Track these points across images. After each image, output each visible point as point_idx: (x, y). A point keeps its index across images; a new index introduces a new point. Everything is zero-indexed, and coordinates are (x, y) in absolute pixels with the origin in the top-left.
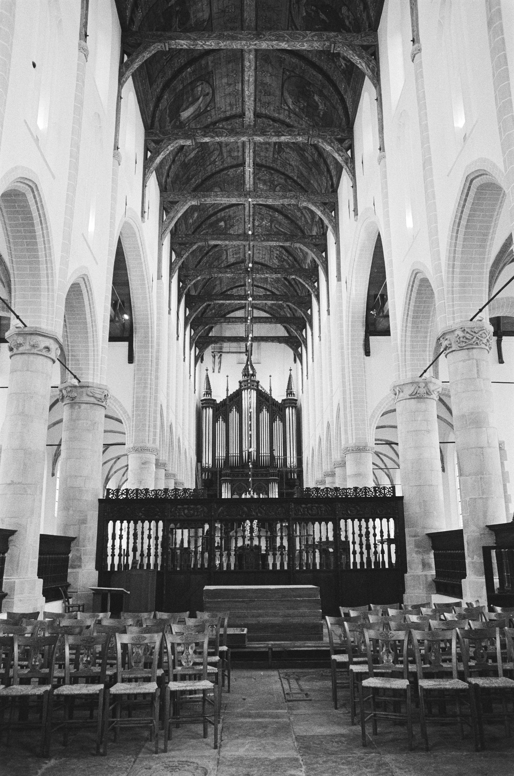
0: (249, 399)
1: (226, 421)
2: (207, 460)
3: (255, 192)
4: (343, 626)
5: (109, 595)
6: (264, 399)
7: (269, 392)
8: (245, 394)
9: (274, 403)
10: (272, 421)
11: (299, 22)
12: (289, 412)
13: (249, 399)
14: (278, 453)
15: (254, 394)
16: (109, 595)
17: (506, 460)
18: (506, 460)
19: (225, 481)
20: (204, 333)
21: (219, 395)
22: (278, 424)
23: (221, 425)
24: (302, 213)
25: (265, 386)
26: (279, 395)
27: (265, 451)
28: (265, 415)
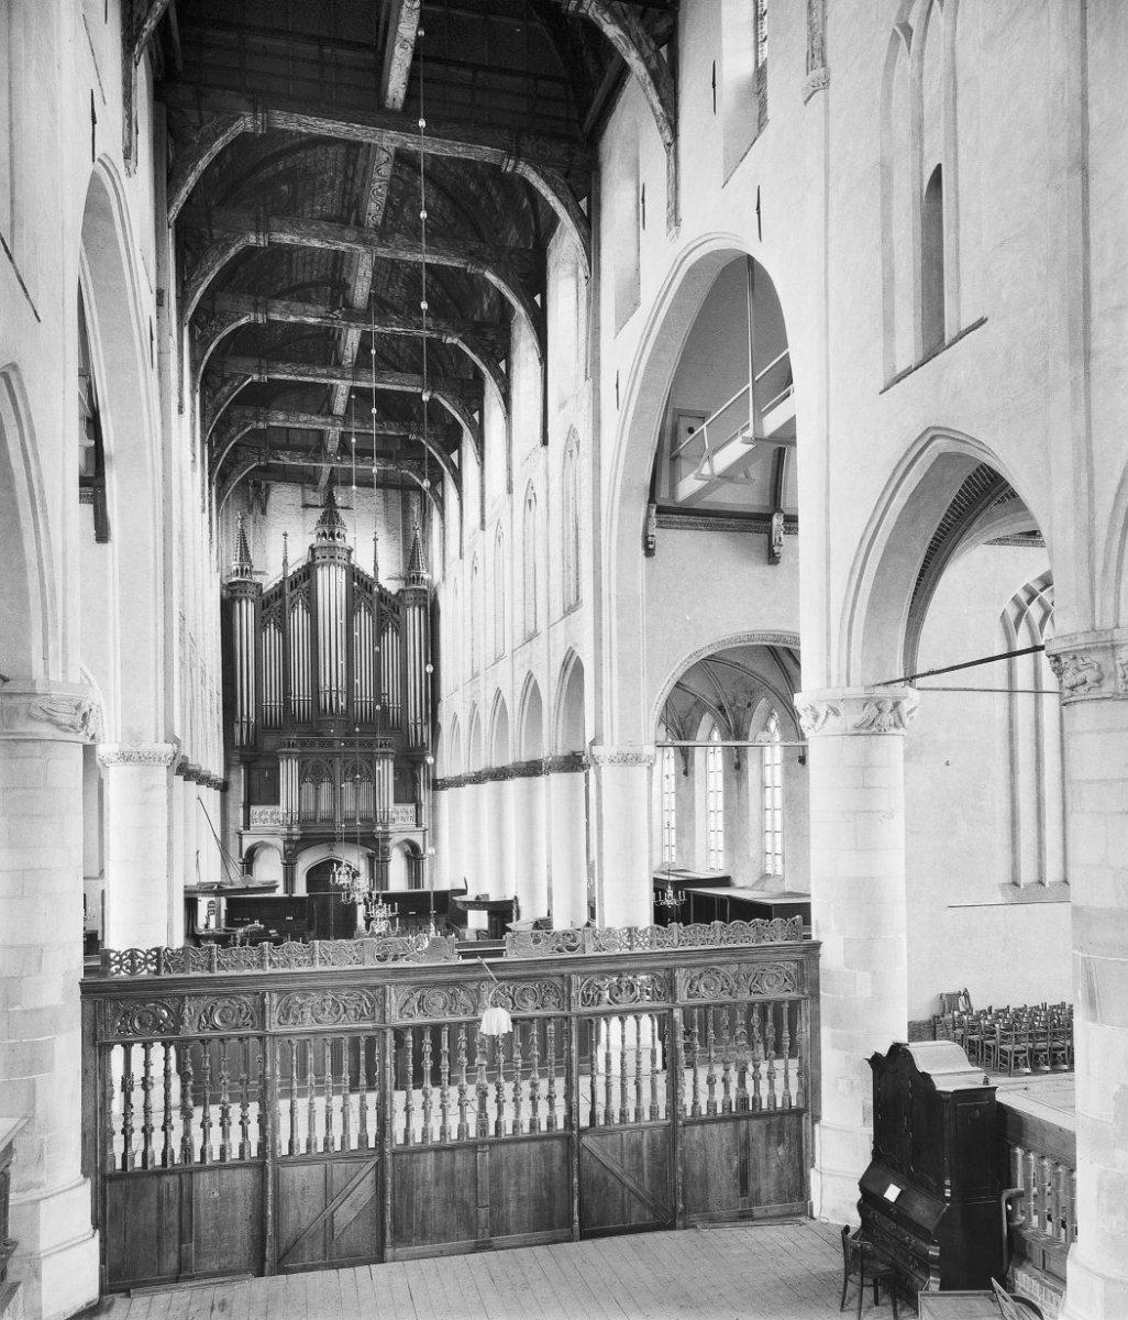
0: (331, 586)
1: (283, 628)
2: (247, 708)
3: (402, 120)
4: (937, 1264)
5: (396, 84)
6: (360, 586)
7: (372, 575)
8: (322, 575)
9: (383, 596)
10: (380, 632)
11: (365, 147)
12: (414, 617)
13: (331, 586)
14: (391, 687)
15: (342, 576)
16: (396, 84)
17: (488, 895)
18: (488, 895)
19: (289, 755)
20: (244, 468)
21: (270, 575)
22: (390, 638)
23: (272, 635)
24: (482, 185)
25: (363, 562)
26: (388, 577)
27: (364, 681)
28: (365, 622)
